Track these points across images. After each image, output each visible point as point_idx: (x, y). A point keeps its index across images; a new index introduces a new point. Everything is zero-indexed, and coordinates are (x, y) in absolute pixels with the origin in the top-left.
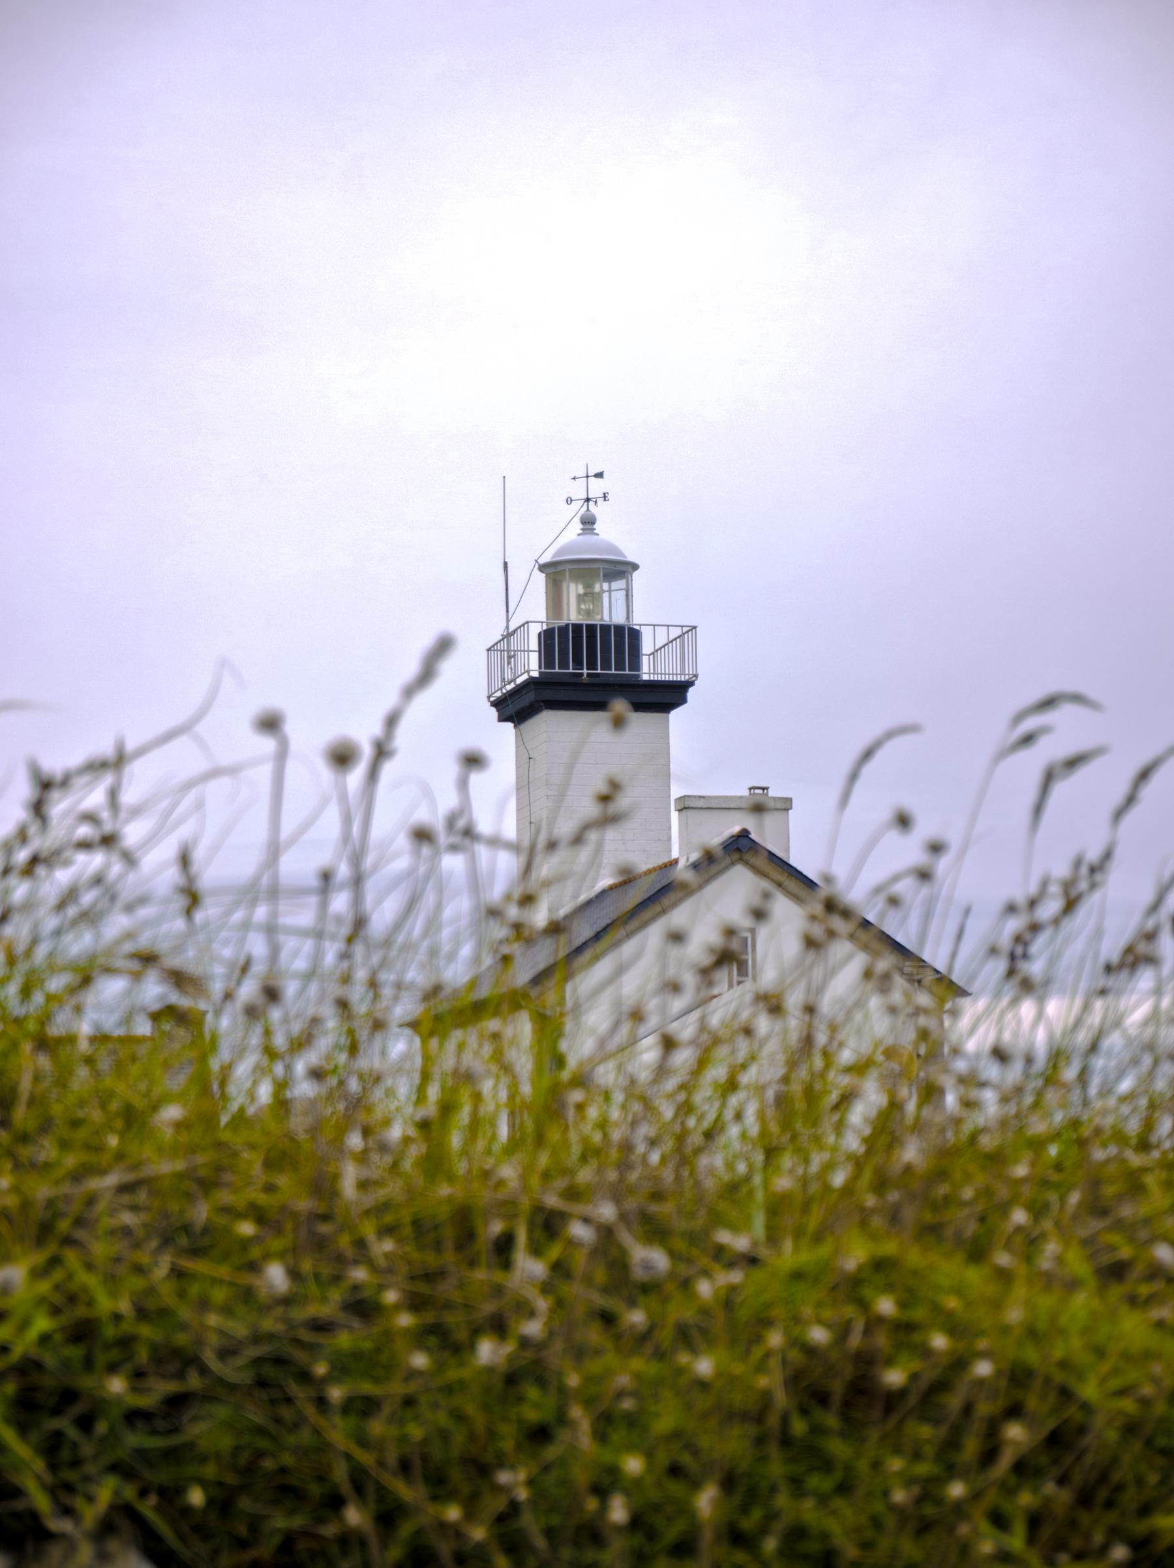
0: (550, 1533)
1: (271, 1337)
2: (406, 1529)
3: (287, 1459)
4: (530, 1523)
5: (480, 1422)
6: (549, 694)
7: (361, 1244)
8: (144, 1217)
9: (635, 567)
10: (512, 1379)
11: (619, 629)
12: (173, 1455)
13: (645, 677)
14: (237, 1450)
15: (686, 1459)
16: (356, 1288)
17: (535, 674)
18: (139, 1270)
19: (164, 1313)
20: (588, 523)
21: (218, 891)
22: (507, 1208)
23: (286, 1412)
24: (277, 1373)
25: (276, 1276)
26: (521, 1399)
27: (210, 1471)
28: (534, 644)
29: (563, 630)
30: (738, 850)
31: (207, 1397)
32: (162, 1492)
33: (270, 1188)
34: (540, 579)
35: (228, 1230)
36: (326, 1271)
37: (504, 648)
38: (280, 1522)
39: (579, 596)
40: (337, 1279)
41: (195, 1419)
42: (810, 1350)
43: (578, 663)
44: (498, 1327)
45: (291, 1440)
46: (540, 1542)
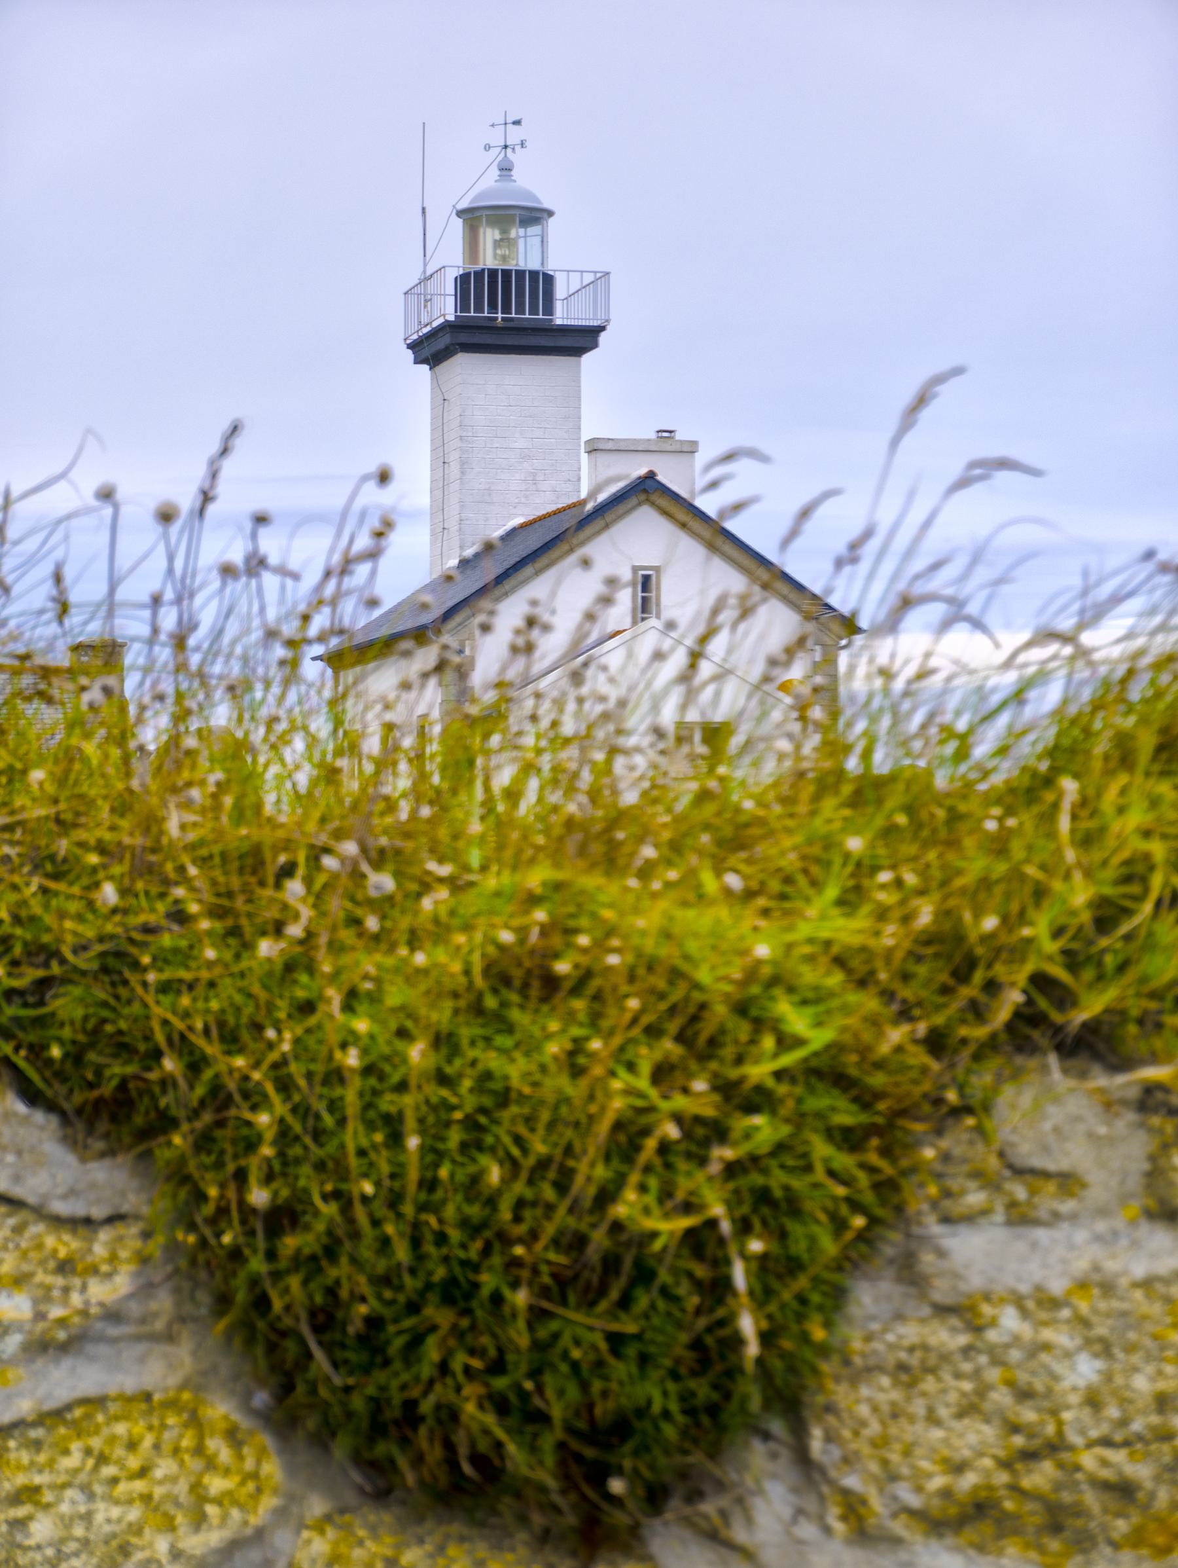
0: (309, 1076)
1: (112, 937)
2: (208, 1074)
3: (123, 1025)
4: (295, 1069)
5: (263, 996)
6: (464, 338)
7: (181, 869)
8: (17, 850)
9: (550, 213)
10: (289, 968)
11: (534, 274)
12: (40, 1022)
13: (559, 322)
14: (86, 1018)
15: (409, 1024)
16: (177, 902)
17: (451, 318)
18: (15, 887)
19: (33, 919)
20: (506, 169)
21: (80, 605)
22: (287, 845)
23: (123, 992)
24: (116, 964)
25: (109, 893)
26: (295, 982)
27: (67, 1033)
28: (450, 289)
29: (479, 274)
30: (645, 491)
31: (65, 981)
32: (31, 1047)
33: (113, 828)
34: (458, 224)
35: (78, 859)
36: (154, 890)
37: (419, 293)
38: (118, 1069)
39: (495, 241)
40: (162, 895)
41: (56, 996)
42: (502, 948)
43: (493, 306)
44: (278, 929)
45: (126, 1011)
46: (302, 1083)
